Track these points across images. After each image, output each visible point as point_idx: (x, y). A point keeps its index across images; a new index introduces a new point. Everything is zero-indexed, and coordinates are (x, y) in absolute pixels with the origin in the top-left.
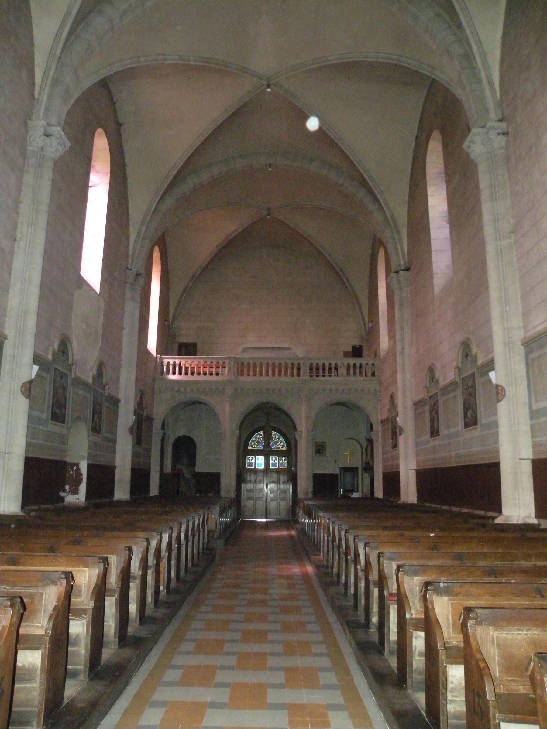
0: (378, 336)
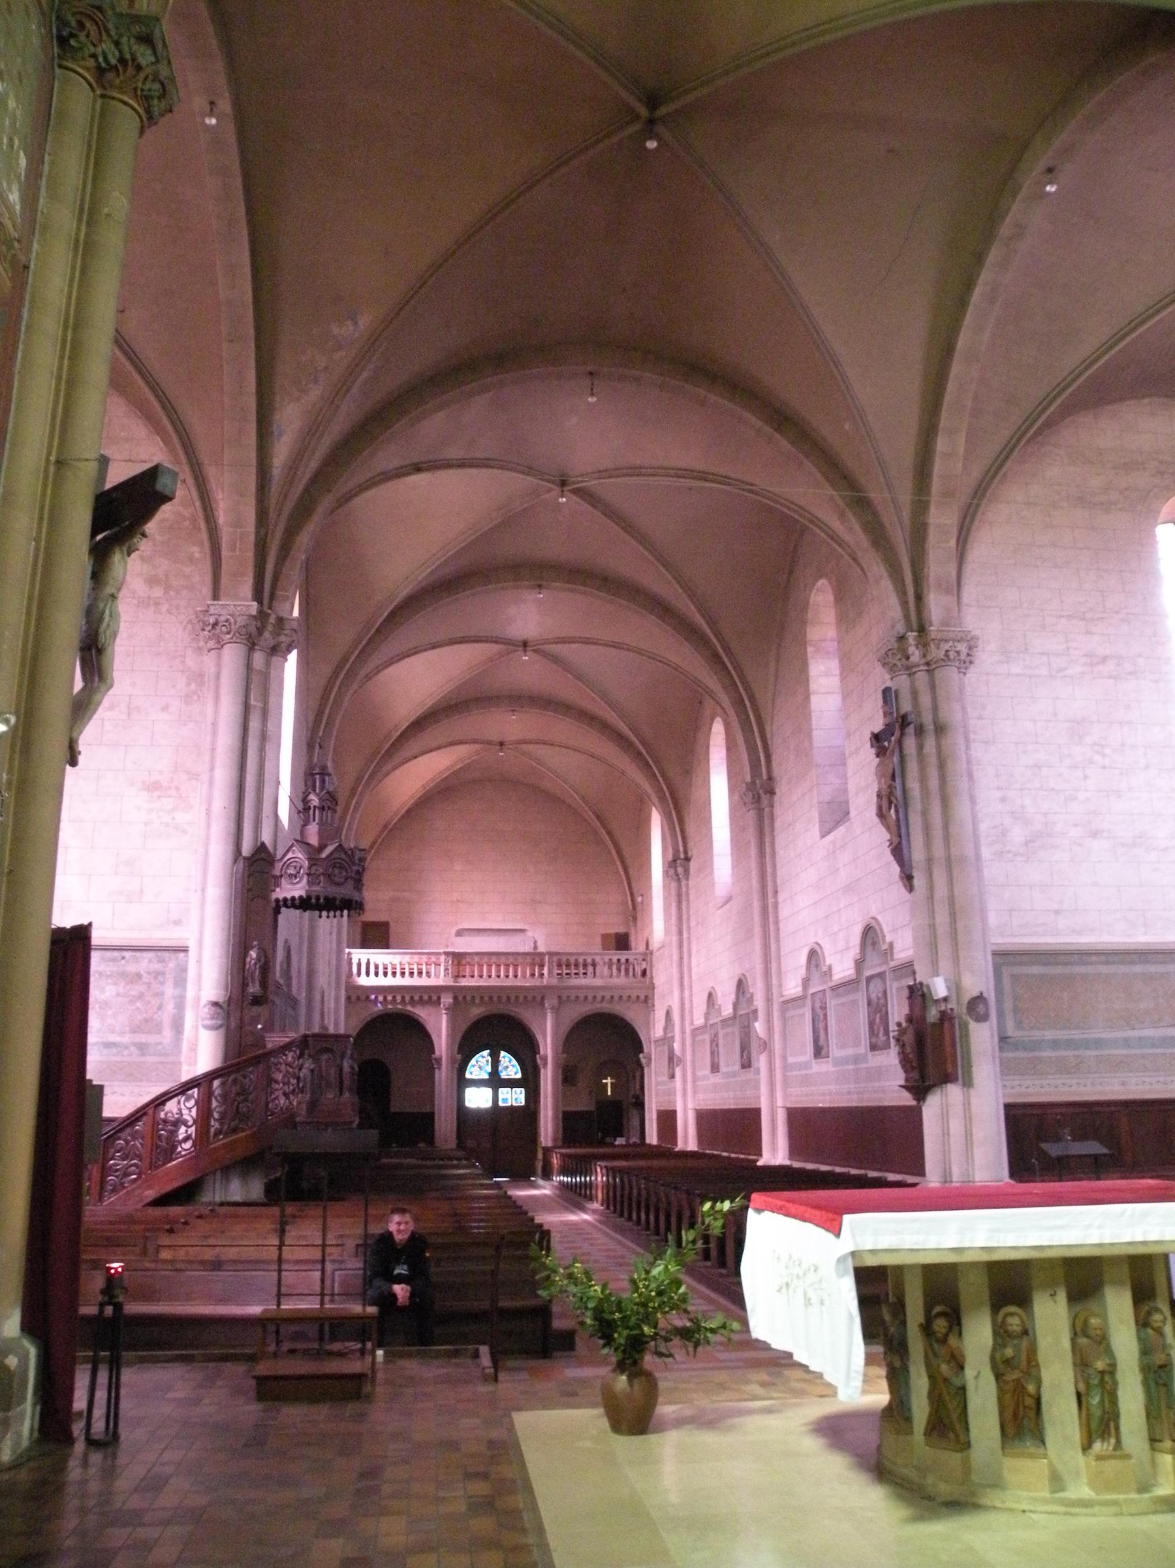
0: (651, 922)
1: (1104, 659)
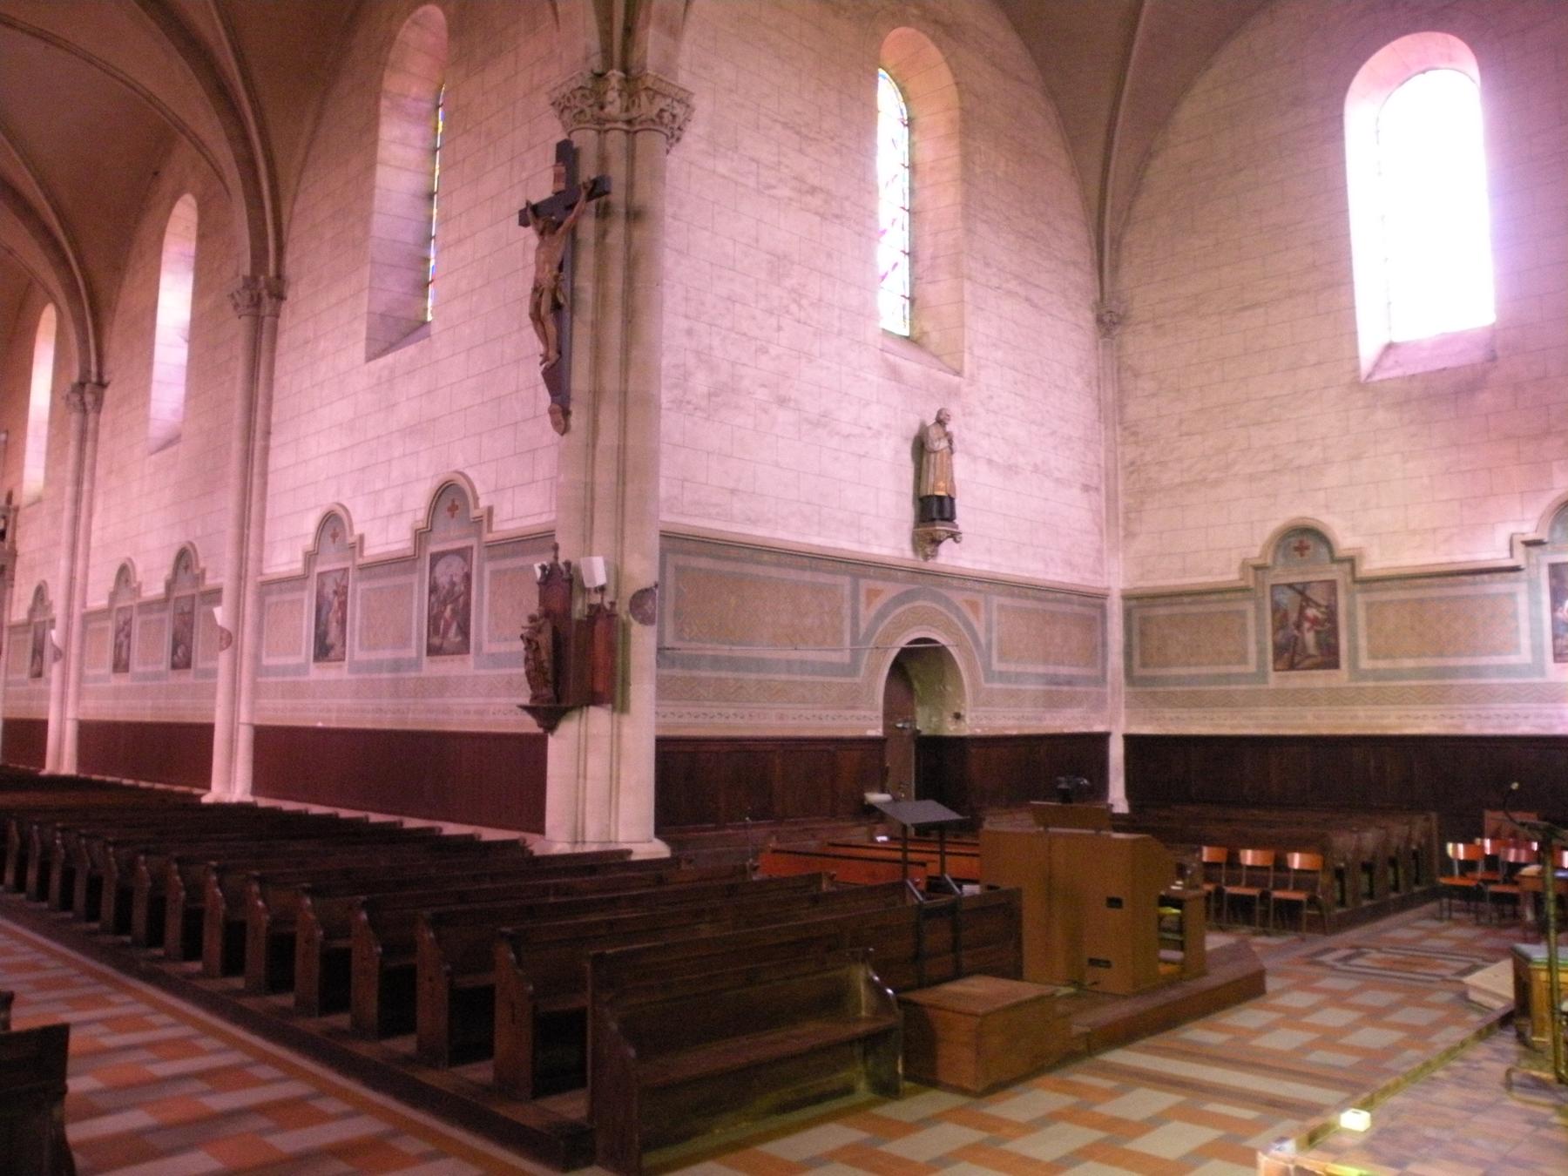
1: (813, 190)
